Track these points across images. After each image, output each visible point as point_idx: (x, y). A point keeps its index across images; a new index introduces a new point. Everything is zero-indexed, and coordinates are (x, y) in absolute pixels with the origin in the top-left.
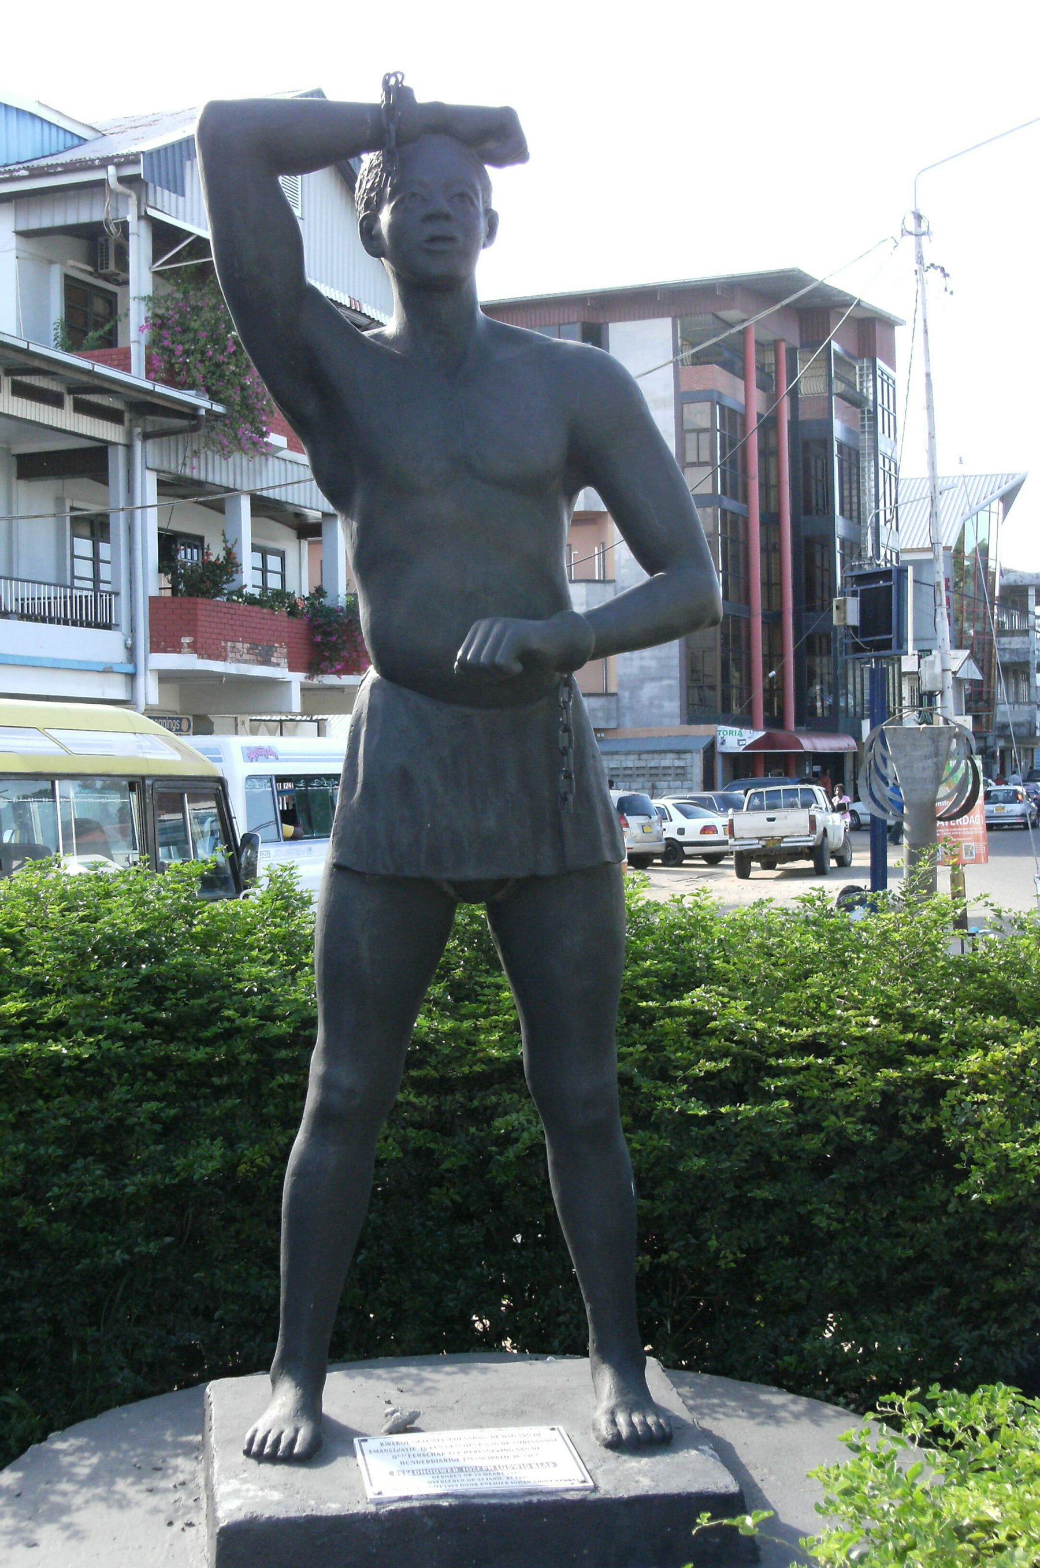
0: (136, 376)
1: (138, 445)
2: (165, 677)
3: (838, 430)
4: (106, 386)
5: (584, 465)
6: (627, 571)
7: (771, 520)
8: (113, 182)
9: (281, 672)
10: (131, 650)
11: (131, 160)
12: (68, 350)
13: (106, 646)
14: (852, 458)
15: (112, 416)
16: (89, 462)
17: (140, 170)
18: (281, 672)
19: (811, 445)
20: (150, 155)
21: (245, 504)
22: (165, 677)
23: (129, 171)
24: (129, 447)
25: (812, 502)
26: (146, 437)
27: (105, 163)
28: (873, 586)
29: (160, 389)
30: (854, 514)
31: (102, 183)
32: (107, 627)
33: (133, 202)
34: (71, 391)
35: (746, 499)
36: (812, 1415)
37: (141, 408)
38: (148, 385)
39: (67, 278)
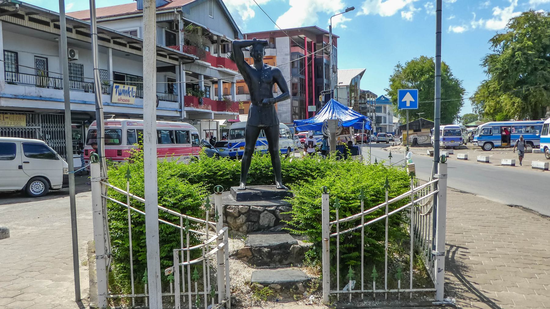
0: (181, 52)
1: (182, 65)
2: (187, 112)
3: (325, 60)
4: (175, 54)
5: (275, 80)
6: (280, 93)
7: (310, 79)
8: (176, 12)
9: (210, 111)
10: (181, 108)
11: (179, 7)
12: (167, 46)
13: (176, 105)
14: (328, 65)
15: (177, 60)
16: (172, 69)
17: (181, 9)
18: (210, 111)
19: (318, 63)
20: (183, 6)
21: (203, 77)
22: (187, 112)
23: (179, 10)
24: (180, 66)
25: (319, 75)
26: (183, 64)
27: (174, 8)
28: (347, 231)
29: (186, 54)
30: (328, 78)
31: (173, 12)
32: (176, 102)
33: (179, 16)
34: (168, 55)
35: (305, 75)
36: (107, 276)
37: (182, 57)
38: (184, 54)
39: (166, 31)
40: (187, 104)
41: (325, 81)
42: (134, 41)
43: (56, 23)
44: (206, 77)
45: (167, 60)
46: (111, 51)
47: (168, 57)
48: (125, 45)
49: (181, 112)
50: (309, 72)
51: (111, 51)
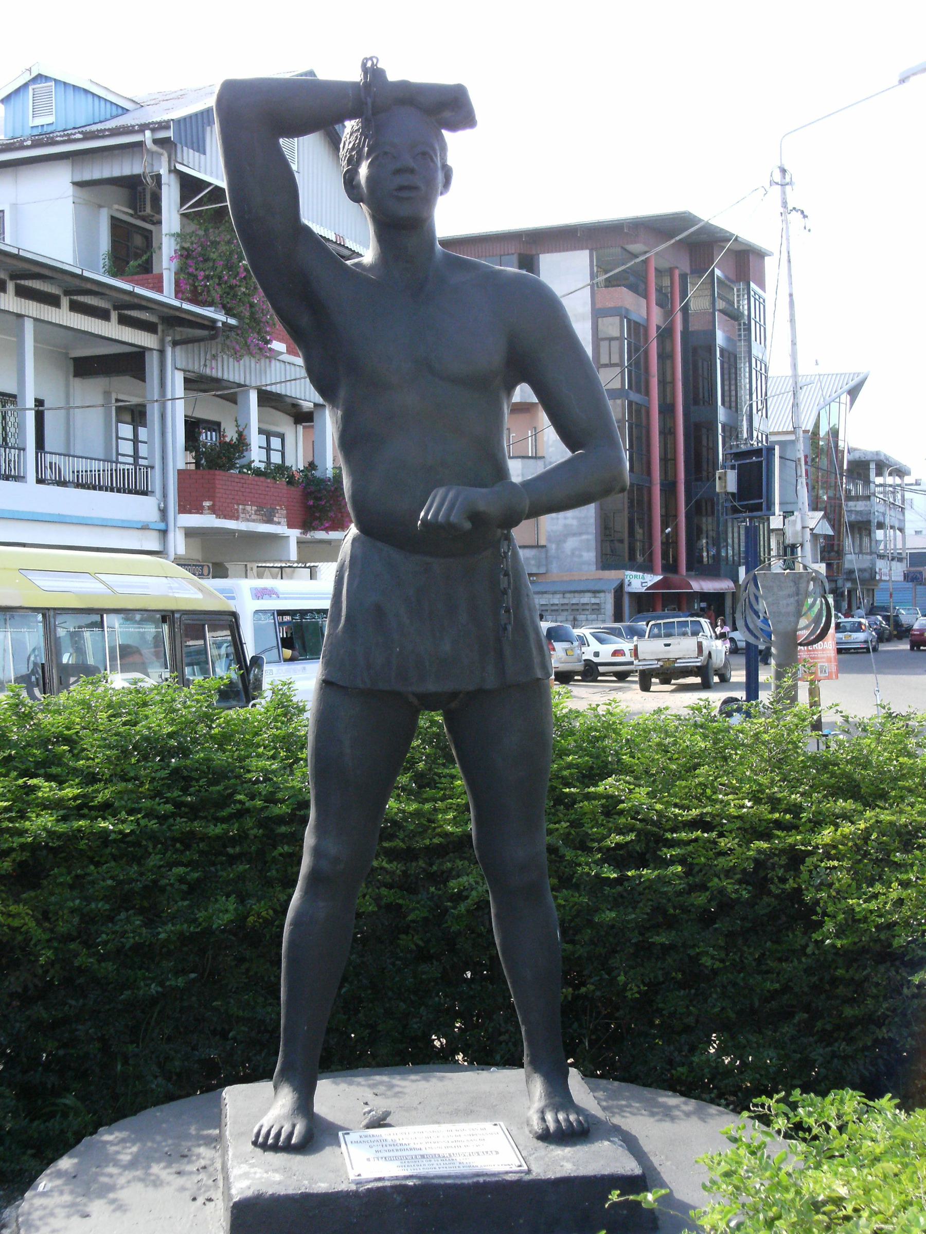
0: (168, 296)
1: (169, 350)
2: (190, 533)
3: (720, 338)
5: (520, 367)
6: (553, 448)
7: (667, 410)
8: (149, 143)
10: (163, 512)
12: (114, 275)
16: (131, 363)
17: (170, 134)
19: (699, 351)
20: (178, 122)
21: (253, 397)
22: (190, 533)
23: (162, 135)
24: (162, 352)
26: (175, 344)
27: (143, 128)
30: (733, 405)
31: (140, 144)
32: (145, 493)
33: (165, 159)
34: (116, 308)
35: (647, 393)
37: (171, 322)
38: (177, 303)
40: (188, 505)
41: (722, 414)
42: (89, 286)
43: (22, 282)
44: (268, 399)
45: (112, 329)
46: (29, 326)
47: (65, 302)
48: (103, 315)
49: (164, 533)
50: (663, 383)
51: (29, 326)
